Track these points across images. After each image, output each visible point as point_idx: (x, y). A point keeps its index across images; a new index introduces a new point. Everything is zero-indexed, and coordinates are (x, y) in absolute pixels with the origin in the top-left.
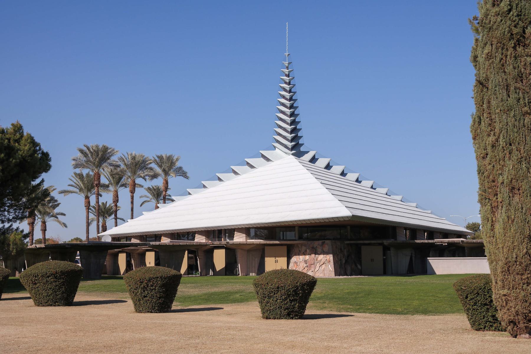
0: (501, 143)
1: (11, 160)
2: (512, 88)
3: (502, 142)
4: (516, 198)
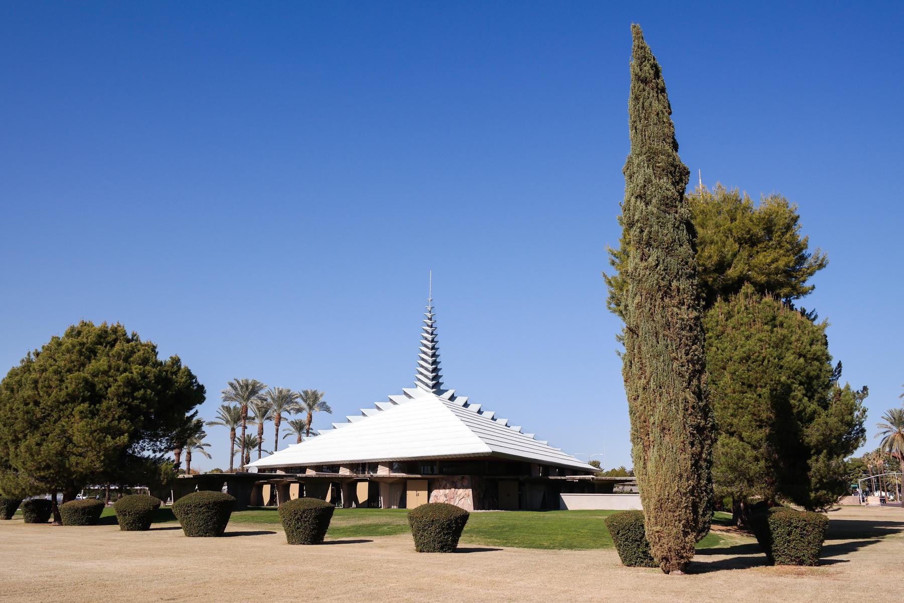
0: (652, 386)
1: (167, 392)
2: (661, 336)
3: (652, 385)
4: (667, 438)
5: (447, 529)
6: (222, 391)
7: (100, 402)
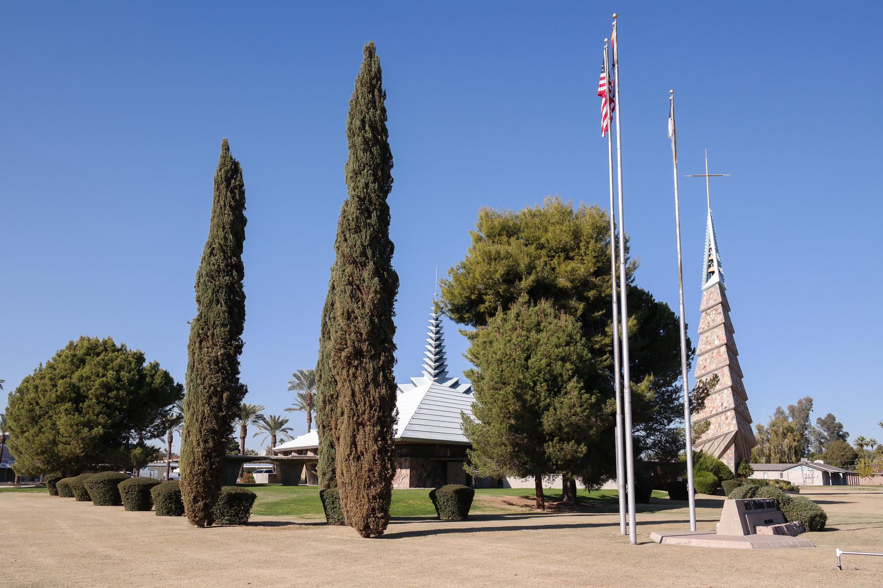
1: (140, 391)
5: (169, 499)
6: (288, 381)
7: (84, 402)
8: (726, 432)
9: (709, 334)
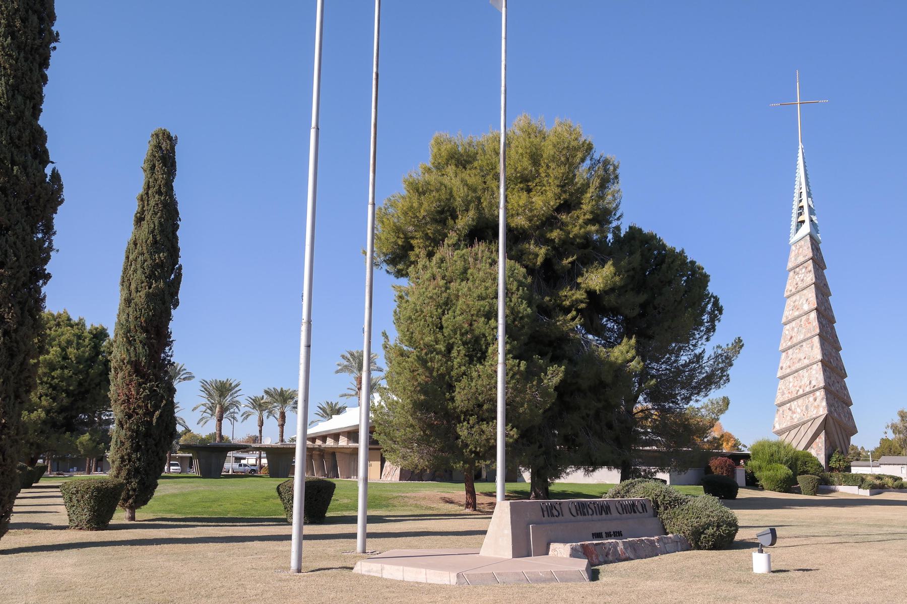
6: (337, 363)
8: (814, 416)
9: (797, 297)
